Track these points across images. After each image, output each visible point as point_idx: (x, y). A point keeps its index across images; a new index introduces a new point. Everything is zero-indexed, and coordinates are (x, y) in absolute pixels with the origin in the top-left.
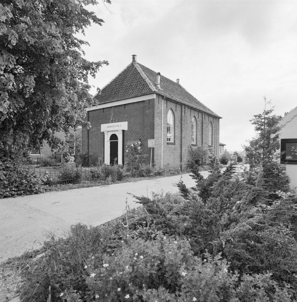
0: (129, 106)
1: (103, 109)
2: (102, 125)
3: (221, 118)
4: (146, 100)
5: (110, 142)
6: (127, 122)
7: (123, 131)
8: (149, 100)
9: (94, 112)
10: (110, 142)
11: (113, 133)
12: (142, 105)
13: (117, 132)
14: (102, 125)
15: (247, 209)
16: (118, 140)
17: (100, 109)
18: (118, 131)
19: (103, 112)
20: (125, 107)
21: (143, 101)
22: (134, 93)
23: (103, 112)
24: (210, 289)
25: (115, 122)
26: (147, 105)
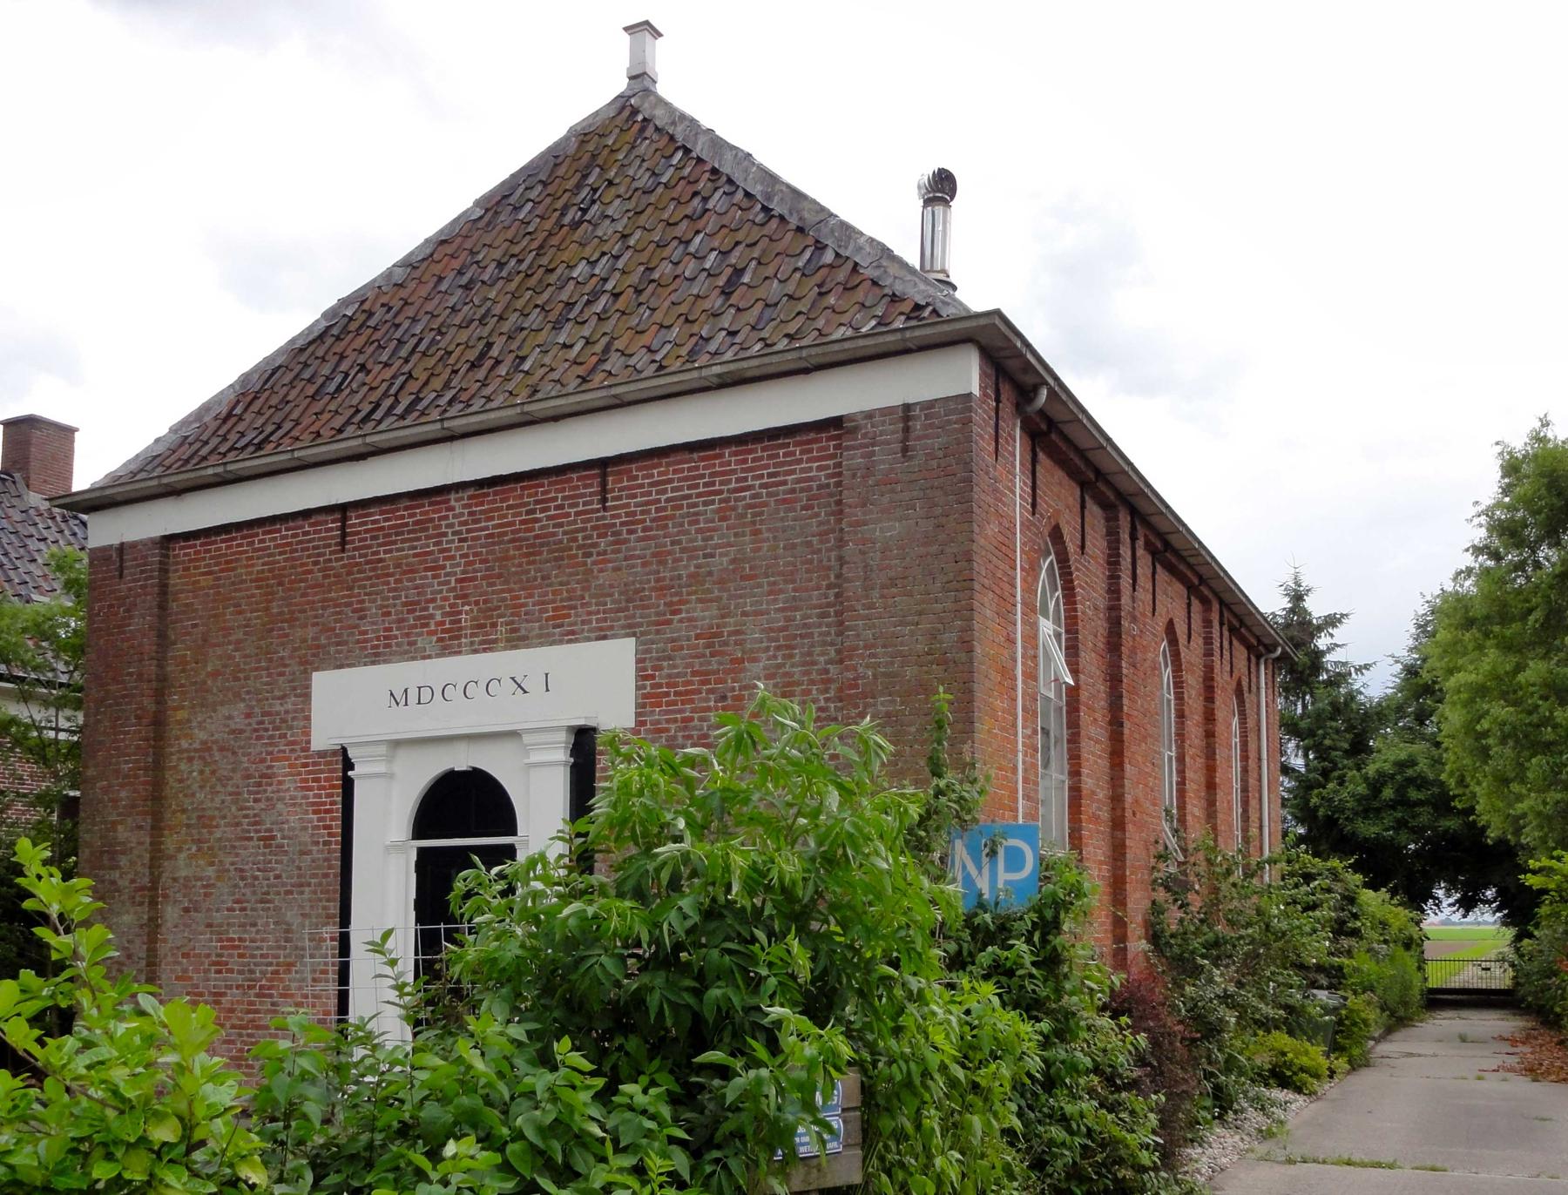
0: (640, 475)
1: (343, 509)
2: (322, 681)
3: (77, 430)
4: (869, 415)
5: (414, 857)
6: (629, 645)
7: (584, 742)
8: (907, 407)
9: (239, 542)
10: (422, 852)
11: (462, 760)
12: (809, 468)
13: (508, 747)
14: (322, 681)
15: (1260, 1131)
16: (512, 831)
17: (306, 514)
18: (514, 734)
19: (343, 543)
20: (604, 485)
21: (836, 423)
22: (403, 353)
23: (343, 543)
24: (220, 965)
25: (488, 646)
26: (885, 459)
